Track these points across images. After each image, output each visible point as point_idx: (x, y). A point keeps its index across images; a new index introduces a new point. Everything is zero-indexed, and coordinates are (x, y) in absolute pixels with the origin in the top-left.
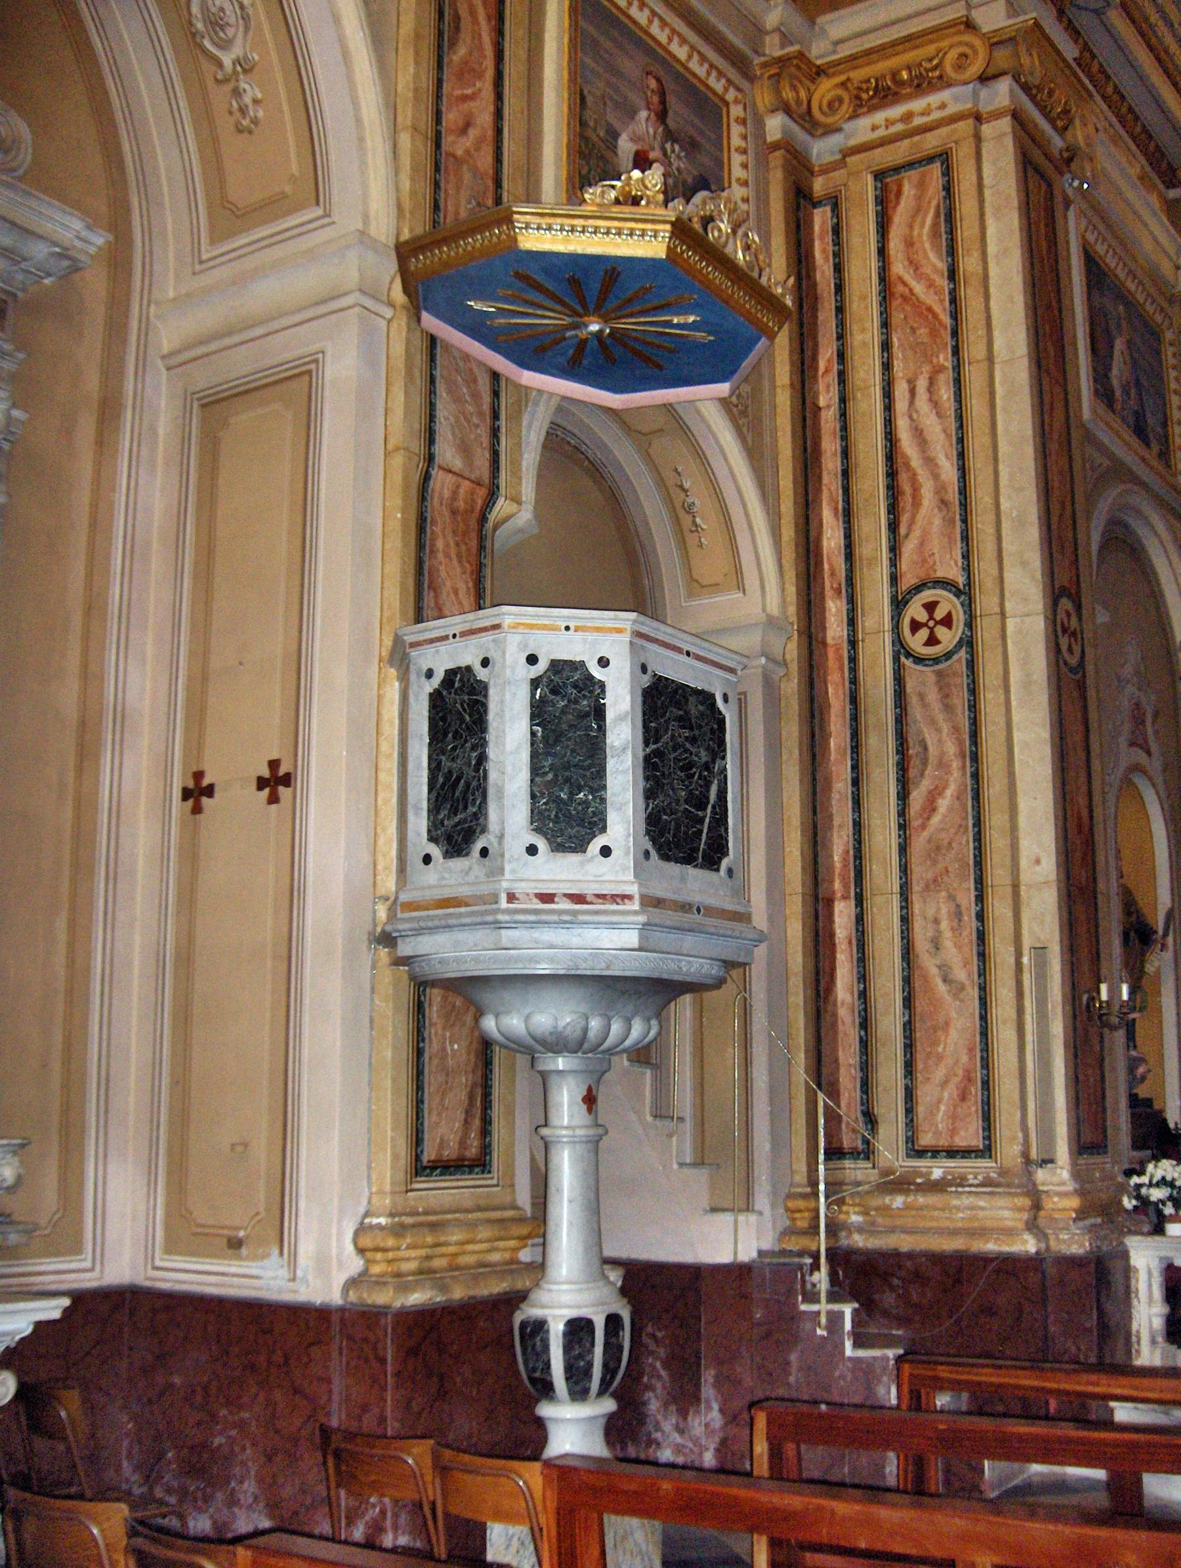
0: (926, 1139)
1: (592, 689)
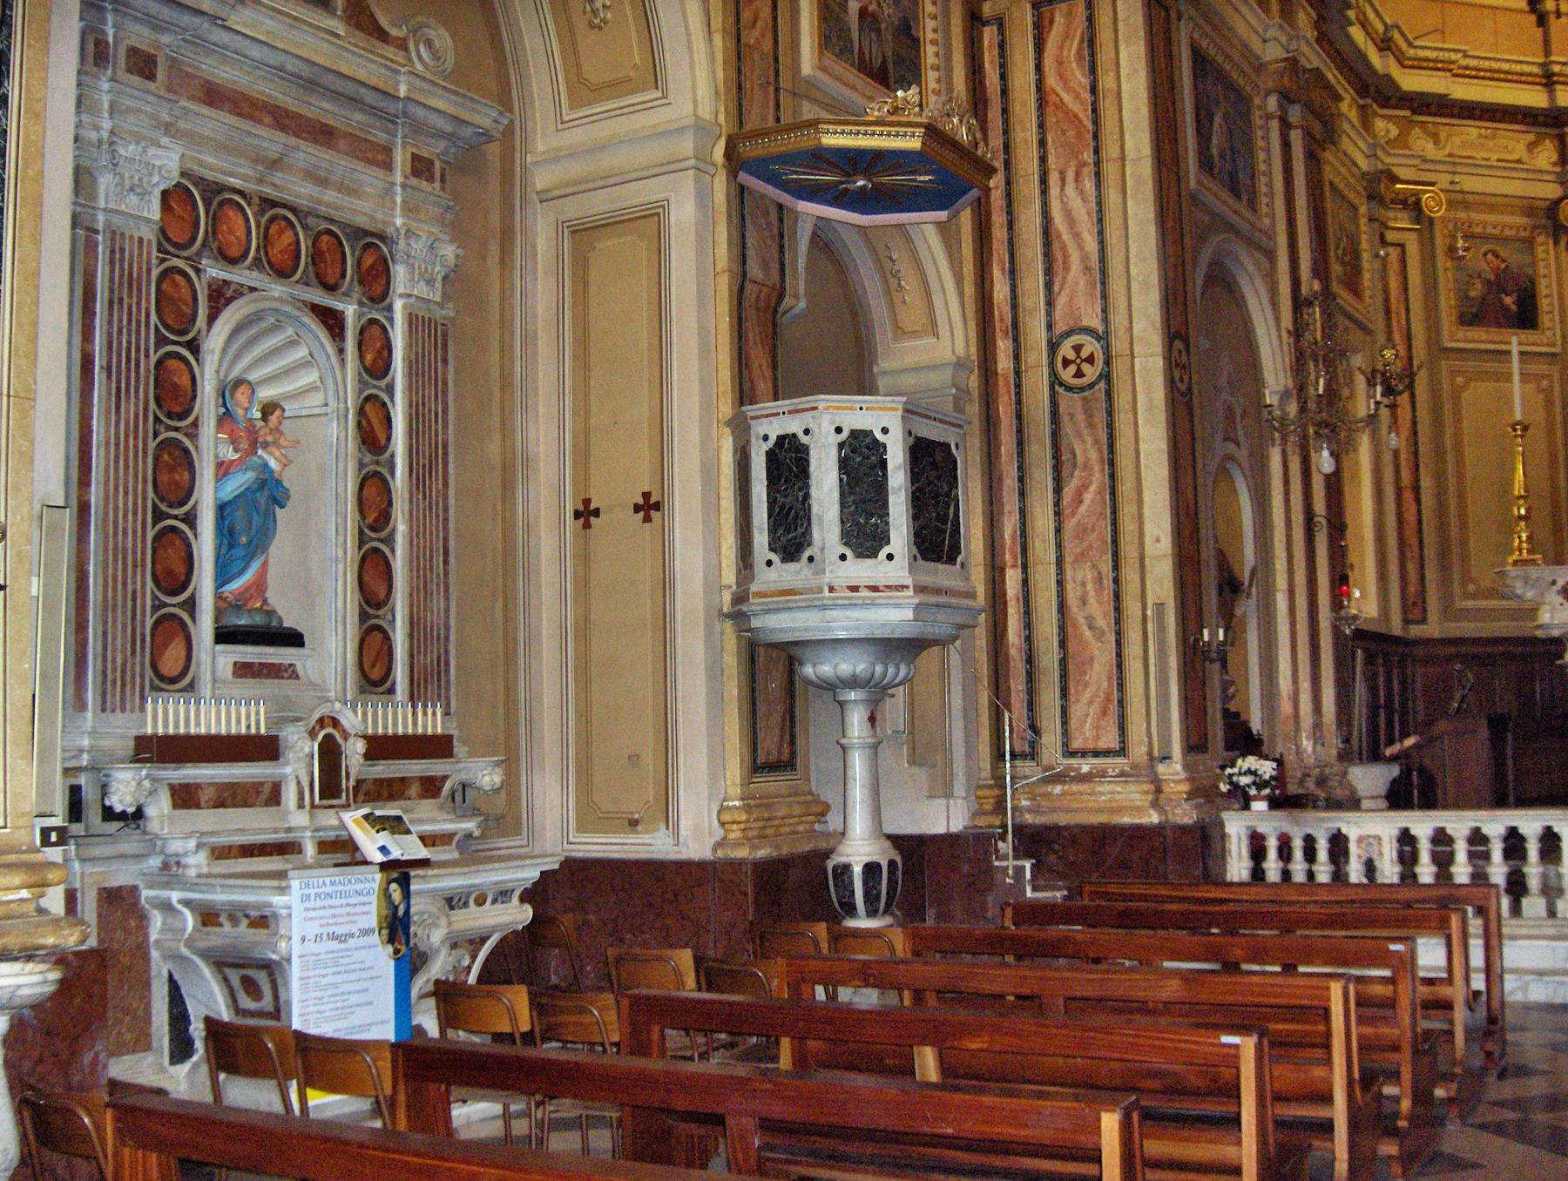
0: (1076, 744)
1: (878, 448)
